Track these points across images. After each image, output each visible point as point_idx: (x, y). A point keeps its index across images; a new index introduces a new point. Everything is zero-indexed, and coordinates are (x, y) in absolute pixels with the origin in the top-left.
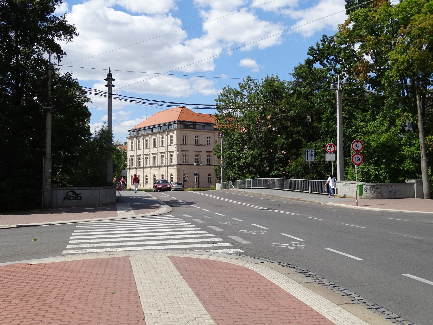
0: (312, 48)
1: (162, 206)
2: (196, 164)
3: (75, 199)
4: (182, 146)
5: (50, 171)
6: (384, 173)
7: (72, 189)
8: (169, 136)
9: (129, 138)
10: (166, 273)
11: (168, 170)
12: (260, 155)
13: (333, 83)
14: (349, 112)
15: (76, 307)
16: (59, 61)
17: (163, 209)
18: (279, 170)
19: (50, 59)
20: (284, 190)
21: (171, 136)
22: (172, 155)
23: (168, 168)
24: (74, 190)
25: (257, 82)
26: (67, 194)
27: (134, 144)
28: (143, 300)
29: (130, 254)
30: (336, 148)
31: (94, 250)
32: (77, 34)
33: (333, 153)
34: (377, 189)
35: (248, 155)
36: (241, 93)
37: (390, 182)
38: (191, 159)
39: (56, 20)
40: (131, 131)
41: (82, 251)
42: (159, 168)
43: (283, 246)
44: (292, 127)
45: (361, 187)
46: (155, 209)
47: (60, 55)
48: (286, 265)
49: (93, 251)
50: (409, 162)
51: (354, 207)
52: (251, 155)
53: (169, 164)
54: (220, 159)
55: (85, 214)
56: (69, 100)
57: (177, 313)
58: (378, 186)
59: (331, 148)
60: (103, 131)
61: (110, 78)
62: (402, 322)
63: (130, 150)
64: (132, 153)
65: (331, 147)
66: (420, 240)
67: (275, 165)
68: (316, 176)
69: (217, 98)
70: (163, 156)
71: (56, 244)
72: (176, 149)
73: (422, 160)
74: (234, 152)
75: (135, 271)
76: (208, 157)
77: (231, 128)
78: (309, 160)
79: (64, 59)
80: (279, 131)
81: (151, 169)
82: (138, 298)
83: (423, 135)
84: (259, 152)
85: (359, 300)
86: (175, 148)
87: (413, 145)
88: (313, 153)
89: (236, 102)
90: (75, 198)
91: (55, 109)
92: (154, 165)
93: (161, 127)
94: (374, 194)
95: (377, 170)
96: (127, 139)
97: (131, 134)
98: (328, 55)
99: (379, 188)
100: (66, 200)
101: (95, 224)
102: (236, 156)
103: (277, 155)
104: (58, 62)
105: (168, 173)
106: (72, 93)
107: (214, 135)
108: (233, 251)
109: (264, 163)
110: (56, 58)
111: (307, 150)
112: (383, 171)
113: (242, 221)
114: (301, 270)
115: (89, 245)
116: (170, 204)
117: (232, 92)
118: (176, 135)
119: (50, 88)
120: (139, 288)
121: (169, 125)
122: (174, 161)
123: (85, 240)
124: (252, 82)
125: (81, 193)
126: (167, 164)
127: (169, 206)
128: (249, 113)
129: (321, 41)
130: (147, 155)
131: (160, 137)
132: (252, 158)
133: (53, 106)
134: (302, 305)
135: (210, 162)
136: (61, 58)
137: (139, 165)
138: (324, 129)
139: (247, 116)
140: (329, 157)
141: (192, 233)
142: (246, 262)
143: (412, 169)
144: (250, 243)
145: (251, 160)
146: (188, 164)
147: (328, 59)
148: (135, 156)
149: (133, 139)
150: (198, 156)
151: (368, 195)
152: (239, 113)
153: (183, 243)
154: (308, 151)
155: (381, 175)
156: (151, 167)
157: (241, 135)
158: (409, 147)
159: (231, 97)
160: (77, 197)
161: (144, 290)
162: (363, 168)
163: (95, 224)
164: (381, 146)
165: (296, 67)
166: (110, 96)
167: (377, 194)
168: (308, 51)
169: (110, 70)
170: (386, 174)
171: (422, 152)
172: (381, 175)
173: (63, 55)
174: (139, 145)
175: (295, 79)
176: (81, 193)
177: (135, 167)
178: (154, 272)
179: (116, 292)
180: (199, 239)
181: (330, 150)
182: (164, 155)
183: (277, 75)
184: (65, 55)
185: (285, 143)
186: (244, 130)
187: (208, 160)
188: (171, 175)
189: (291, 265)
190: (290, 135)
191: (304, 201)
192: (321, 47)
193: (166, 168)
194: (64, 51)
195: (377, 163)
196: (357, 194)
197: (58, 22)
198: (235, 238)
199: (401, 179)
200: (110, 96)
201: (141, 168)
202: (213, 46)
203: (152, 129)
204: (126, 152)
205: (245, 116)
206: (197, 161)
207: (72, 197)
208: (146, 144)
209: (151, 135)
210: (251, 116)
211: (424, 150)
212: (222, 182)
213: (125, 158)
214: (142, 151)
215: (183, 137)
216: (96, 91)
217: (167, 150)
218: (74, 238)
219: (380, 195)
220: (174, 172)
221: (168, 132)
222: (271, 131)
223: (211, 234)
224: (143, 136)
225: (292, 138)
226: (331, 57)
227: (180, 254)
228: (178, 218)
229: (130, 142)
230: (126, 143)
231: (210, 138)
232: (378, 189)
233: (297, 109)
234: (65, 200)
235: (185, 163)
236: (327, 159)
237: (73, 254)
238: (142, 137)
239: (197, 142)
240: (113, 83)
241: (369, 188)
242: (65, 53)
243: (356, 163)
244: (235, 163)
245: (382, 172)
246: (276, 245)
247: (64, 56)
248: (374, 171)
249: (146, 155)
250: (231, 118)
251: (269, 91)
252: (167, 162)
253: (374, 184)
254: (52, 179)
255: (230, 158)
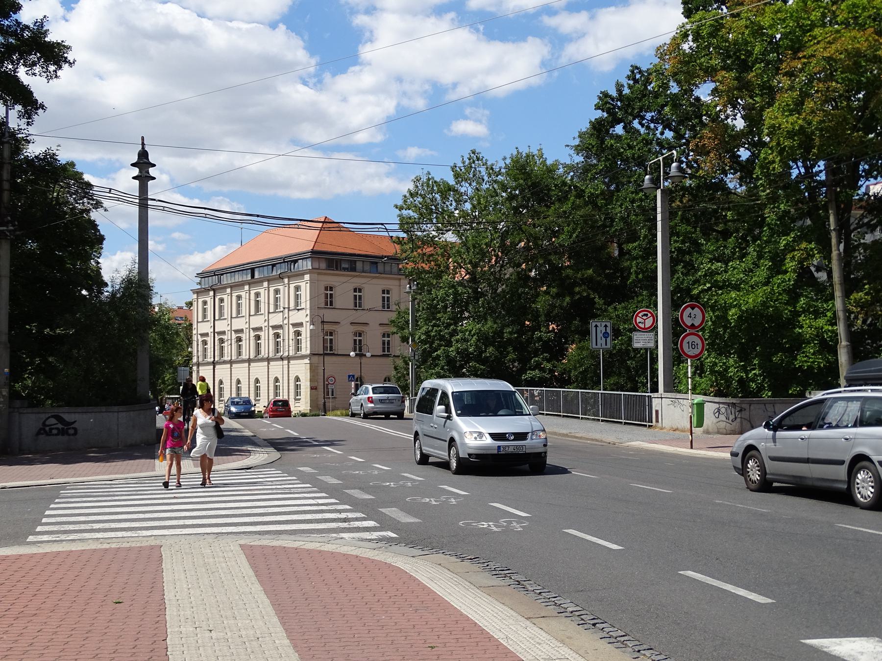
0: (606, 95)
1: (258, 449)
2: (356, 355)
3: (63, 435)
4: (322, 312)
5: (6, 370)
6: (760, 375)
7: (56, 411)
8: (292, 286)
9: (198, 292)
10: (228, 572)
11: (289, 368)
12: (500, 334)
13: (649, 174)
14: (688, 237)
15: (46, 623)
16: (28, 122)
17: (259, 456)
18: (543, 370)
19: (7, 117)
20: (547, 414)
21: (297, 288)
22: (299, 333)
23: (289, 362)
24: (60, 415)
25: (493, 165)
26: (44, 424)
27: (210, 307)
28: (171, 613)
29: (164, 541)
30: (655, 320)
31: (92, 534)
32: (71, 61)
33: (649, 332)
34: (740, 411)
35: (469, 335)
36: (457, 190)
37: (773, 396)
38: (344, 342)
39: (23, 30)
40: (203, 275)
41: (68, 537)
42: (231, 366)
43: (482, 526)
44: (573, 270)
45: (700, 406)
46: (241, 455)
47: (31, 110)
48: (470, 559)
49: (90, 537)
50: (812, 351)
51: (686, 451)
52: (478, 333)
53: (291, 354)
54: (408, 343)
55: (84, 465)
56: (55, 209)
57: (227, 629)
58: (743, 406)
59: (645, 320)
60: (128, 283)
61: (143, 162)
62: (625, 642)
63: (200, 320)
64: (206, 328)
65: (645, 317)
66: (762, 514)
67: (534, 357)
68: (626, 383)
69: (400, 203)
70: (277, 336)
71: (14, 524)
72: (308, 319)
73: (840, 348)
74: (438, 326)
75: (168, 569)
76: (384, 336)
77: (434, 271)
78: (598, 346)
79: (40, 117)
80: (541, 280)
81: (249, 365)
82: (164, 610)
83: (842, 292)
84: (495, 326)
85: (572, 612)
86: (307, 315)
87: (823, 313)
88: (609, 330)
89: (443, 210)
90: (62, 432)
91: (18, 233)
92: (256, 356)
93: (273, 265)
94: (734, 424)
95: (744, 369)
96: (194, 293)
97: (203, 283)
98: (641, 110)
99: (745, 410)
100: (42, 437)
101: (102, 486)
102: (444, 336)
103: (537, 334)
104: (27, 125)
105: (288, 374)
106: (58, 195)
107: (398, 284)
108: (375, 535)
109: (508, 353)
110: (23, 116)
111: (594, 324)
112: (758, 372)
113: (421, 480)
114: (494, 567)
115: (83, 527)
116: (279, 445)
117: (435, 188)
118: (308, 285)
119: (6, 186)
120: (169, 595)
121: (292, 261)
122: (303, 345)
123: (77, 517)
124: (482, 164)
125: (75, 421)
126: (286, 354)
127: (275, 449)
128: (473, 237)
129: (628, 77)
130: (241, 331)
131: (272, 289)
132: (478, 340)
133: (13, 225)
134: (461, 619)
135: (388, 348)
136: (34, 117)
137: (222, 355)
138: (637, 277)
139: (470, 244)
140: (640, 341)
141: (305, 503)
142: (393, 554)
143: (819, 366)
144: (417, 520)
145: (476, 345)
146: (336, 353)
147: (643, 118)
148: (212, 334)
149: (207, 293)
150: (360, 335)
151: (722, 425)
152: (450, 237)
153: (280, 521)
154: (596, 326)
155: (753, 380)
156: (249, 361)
157: (453, 286)
158: (813, 317)
159: (433, 200)
160: (67, 428)
161: (177, 598)
162: (715, 364)
163: (102, 486)
164: (750, 318)
165: (584, 130)
166: (143, 203)
167: (741, 423)
168: (597, 101)
169: (143, 144)
170: (764, 380)
171: (841, 328)
172: (753, 380)
173: (37, 109)
174: (221, 308)
175: (582, 159)
176: (75, 421)
177: (212, 359)
178: (204, 570)
179: (124, 601)
180: (314, 515)
181: (642, 323)
182: (280, 331)
183: (541, 149)
184: (43, 109)
185: (556, 307)
186: (463, 274)
187: (384, 343)
188: (297, 379)
189: (478, 559)
190: (566, 287)
191: (581, 438)
192: (626, 91)
193: (286, 362)
194: (40, 102)
195: (744, 355)
196: (691, 422)
197: (26, 34)
198: (392, 512)
199: (796, 390)
200: (143, 203)
201: (225, 362)
202: (378, 90)
203: (253, 271)
204: (191, 325)
205: (464, 244)
206: (358, 346)
207: (57, 429)
208: (238, 305)
209: (249, 284)
210: (479, 244)
211: (845, 326)
212: (412, 397)
213: (188, 339)
214: (229, 322)
215: (326, 289)
216: (110, 191)
217: (287, 320)
218: (54, 512)
219: (746, 424)
220: (304, 371)
221: (289, 277)
222: (523, 278)
223: (345, 504)
224: (231, 287)
225: (572, 294)
226: (648, 116)
227: (266, 541)
228: (286, 475)
229: (200, 301)
230: (190, 304)
231: (388, 292)
232: (743, 412)
233: (574, 230)
234: (41, 437)
235: (329, 352)
236: (636, 345)
237: (48, 542)
238: (228, 290)
239: (358, 302)
240: (152, 171)
241: (723, 410)
242: (43, 106)
243: (689, 353)
244: (439, 352)
245: (755, 374)
246: (468, 524)
247: (40, 111)
248: (737, 371)
249: (237, 331)
250: (431, 246)
251: (521, 185)
252: (288, 348)
253: (734, 401)
254: (10, 389)
255: (429, 339)
